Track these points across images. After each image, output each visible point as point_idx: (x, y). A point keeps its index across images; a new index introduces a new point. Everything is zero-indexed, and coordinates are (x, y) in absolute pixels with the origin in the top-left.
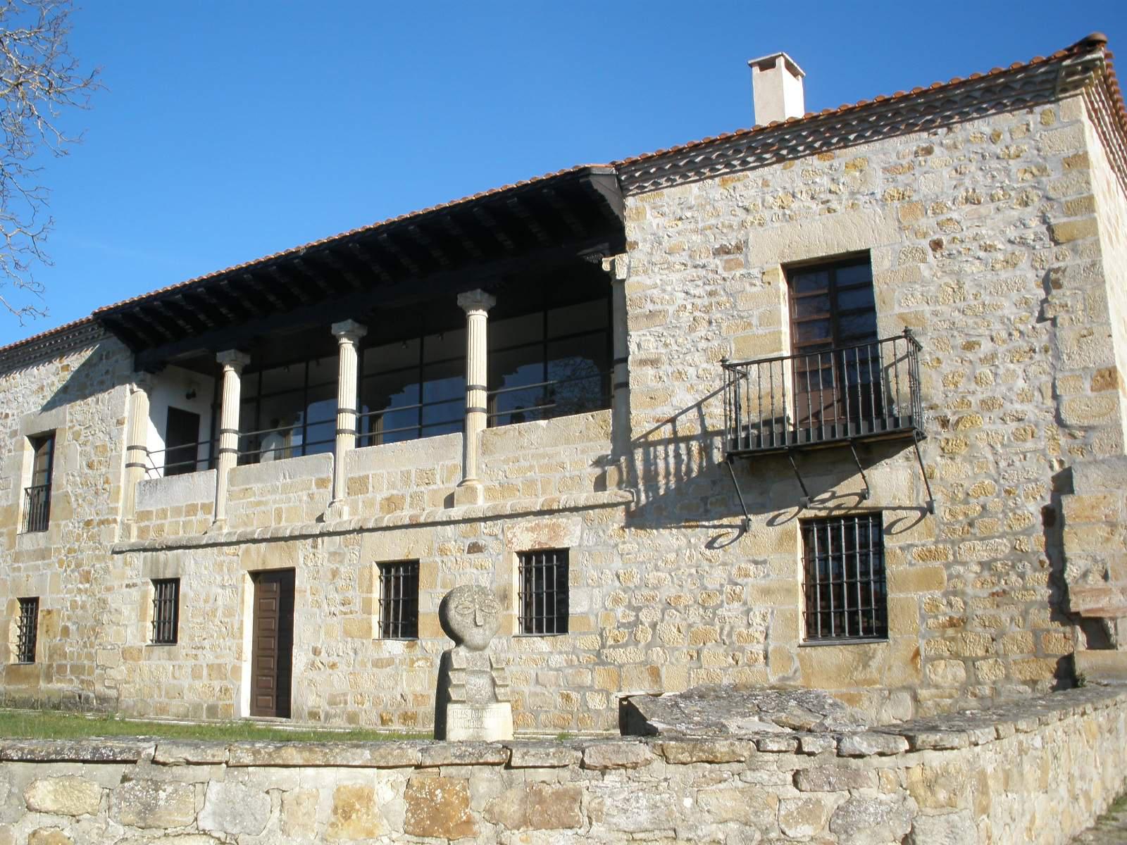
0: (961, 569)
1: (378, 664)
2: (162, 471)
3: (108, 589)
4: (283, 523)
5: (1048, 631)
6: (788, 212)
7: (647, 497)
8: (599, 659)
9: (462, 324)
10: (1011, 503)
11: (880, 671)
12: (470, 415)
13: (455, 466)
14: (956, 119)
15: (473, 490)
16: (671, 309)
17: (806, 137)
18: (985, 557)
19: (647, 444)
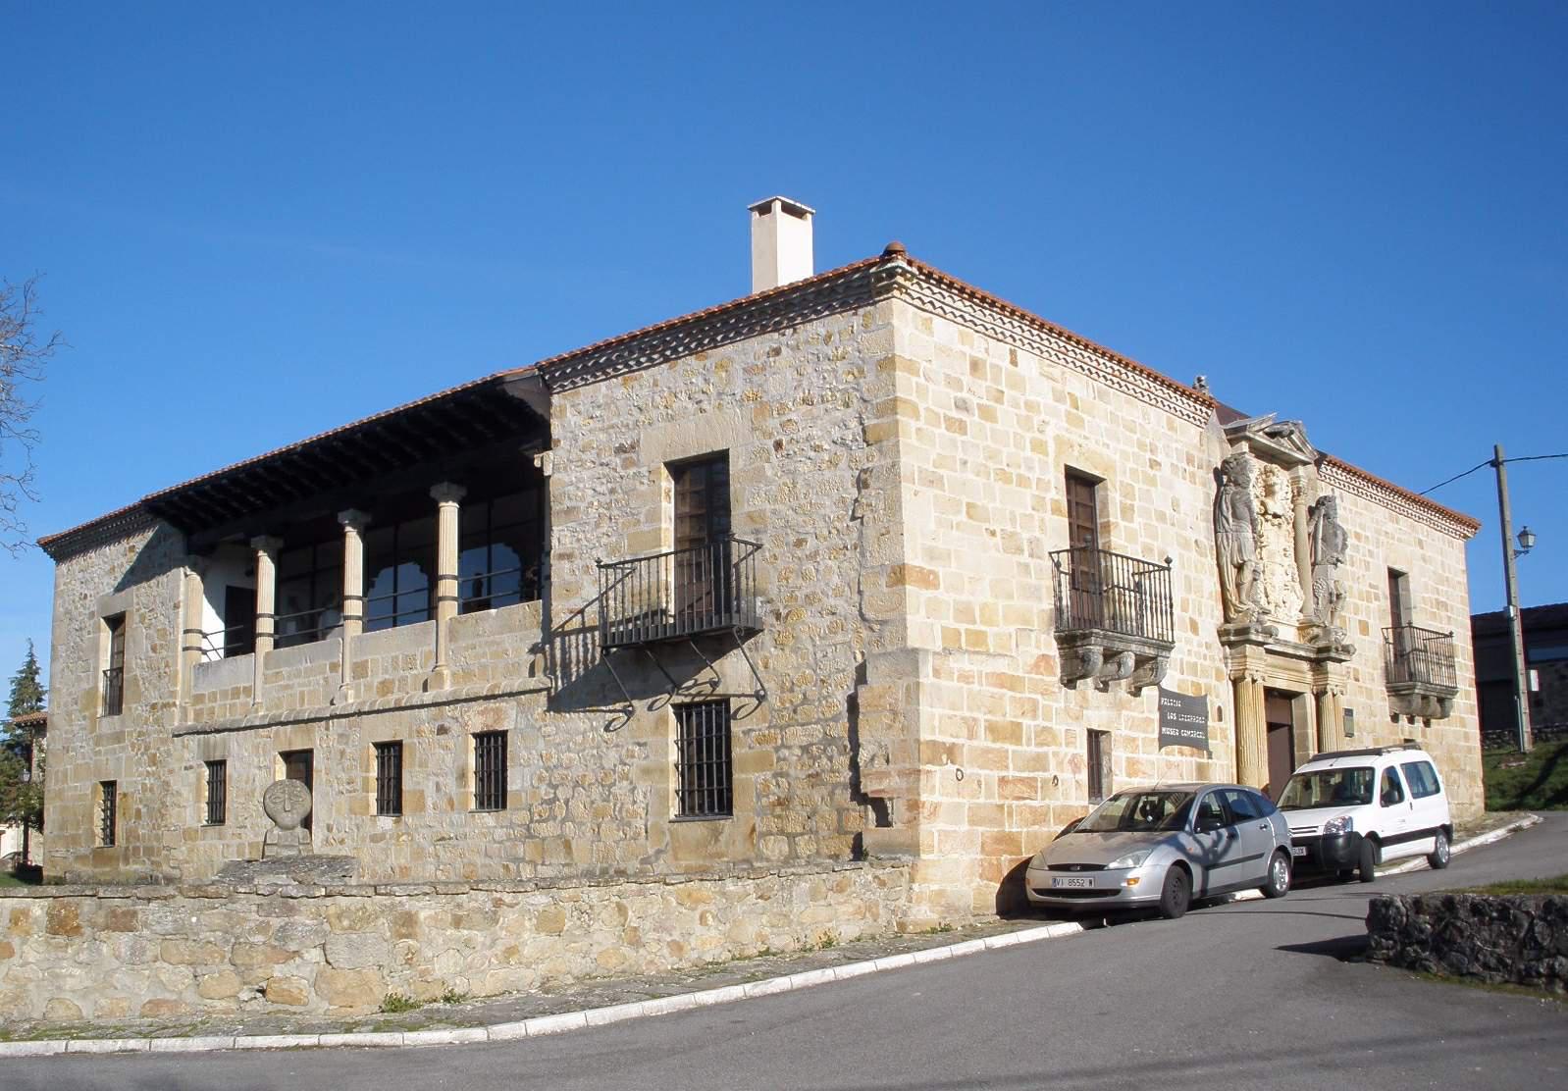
0: (786, 752)
1: (375, 839)
2: (222, 652)
3: (171, 772)
4: (306, 706)
5: (848, 810)
6: (670, 412)
7: (563, 683)
9: (434, 512)
10: (824, 692)
11: (727, 846)
12: (441, 603)
14: (799, 320)
15: (441, 675)
16: (583, 506)
17: (683, 339)
18: (804, 741)
19: (564, 634)
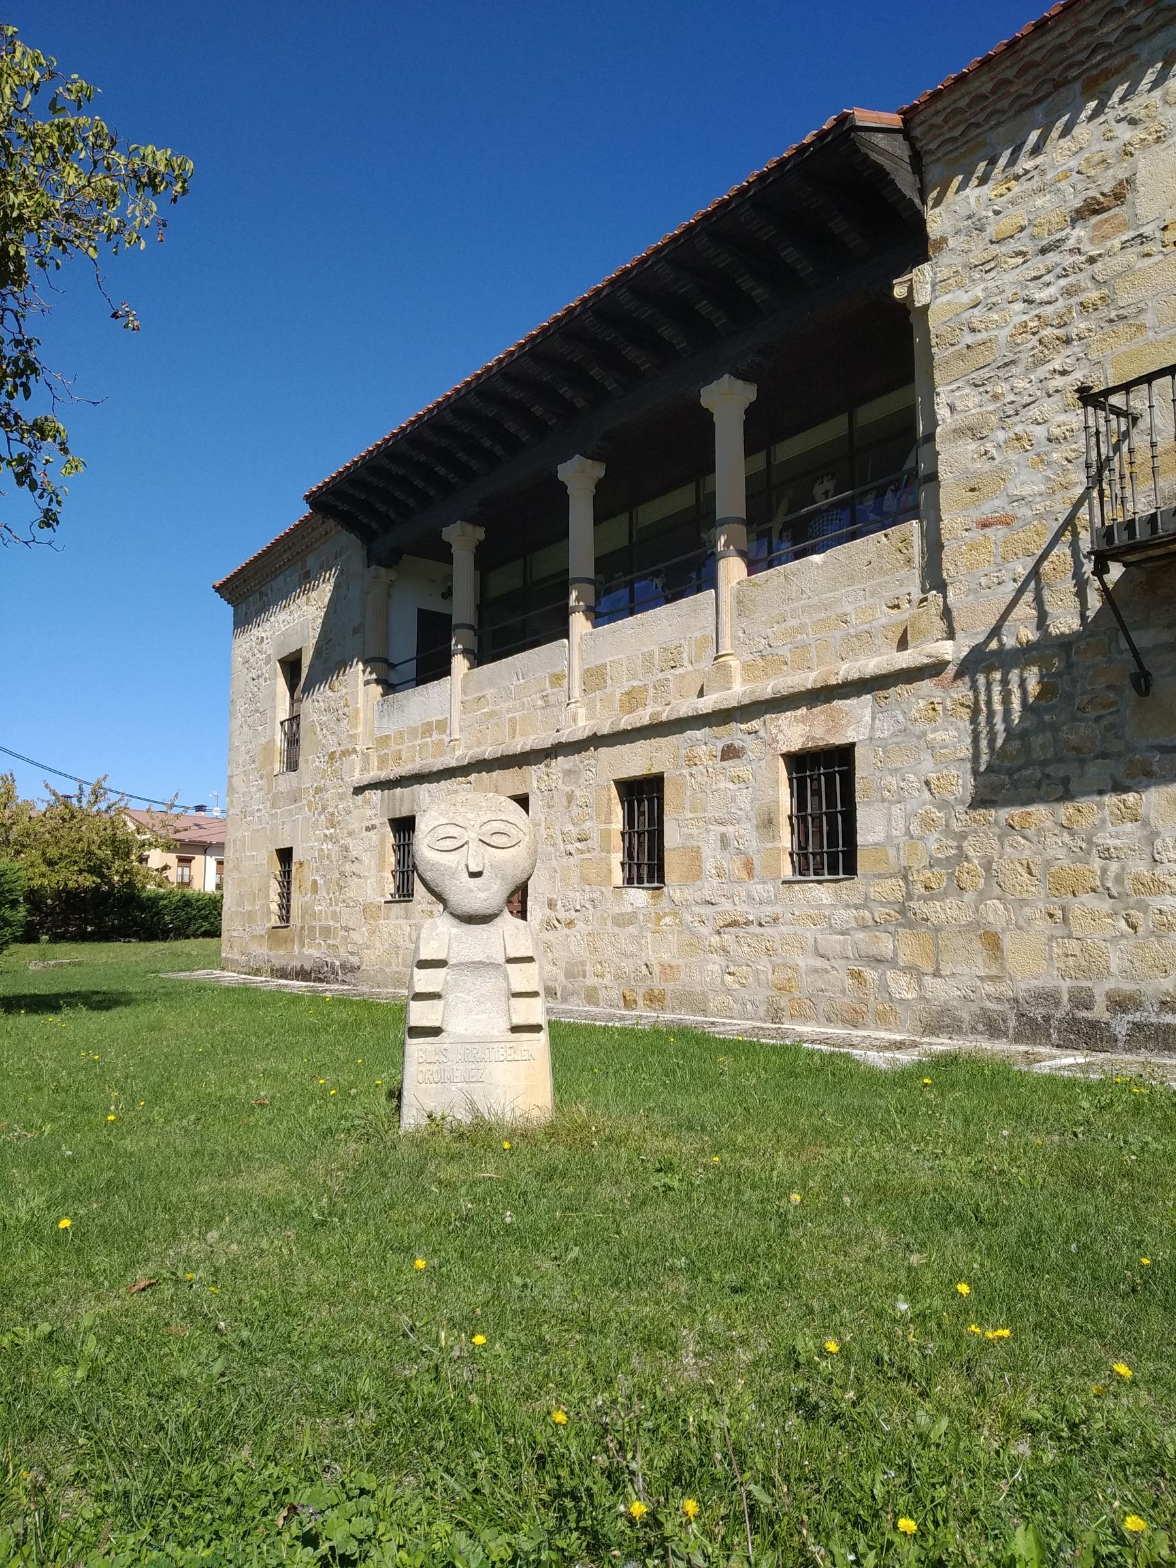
1: (622, 921)
8: (904, 916)
13: (705, 637)
